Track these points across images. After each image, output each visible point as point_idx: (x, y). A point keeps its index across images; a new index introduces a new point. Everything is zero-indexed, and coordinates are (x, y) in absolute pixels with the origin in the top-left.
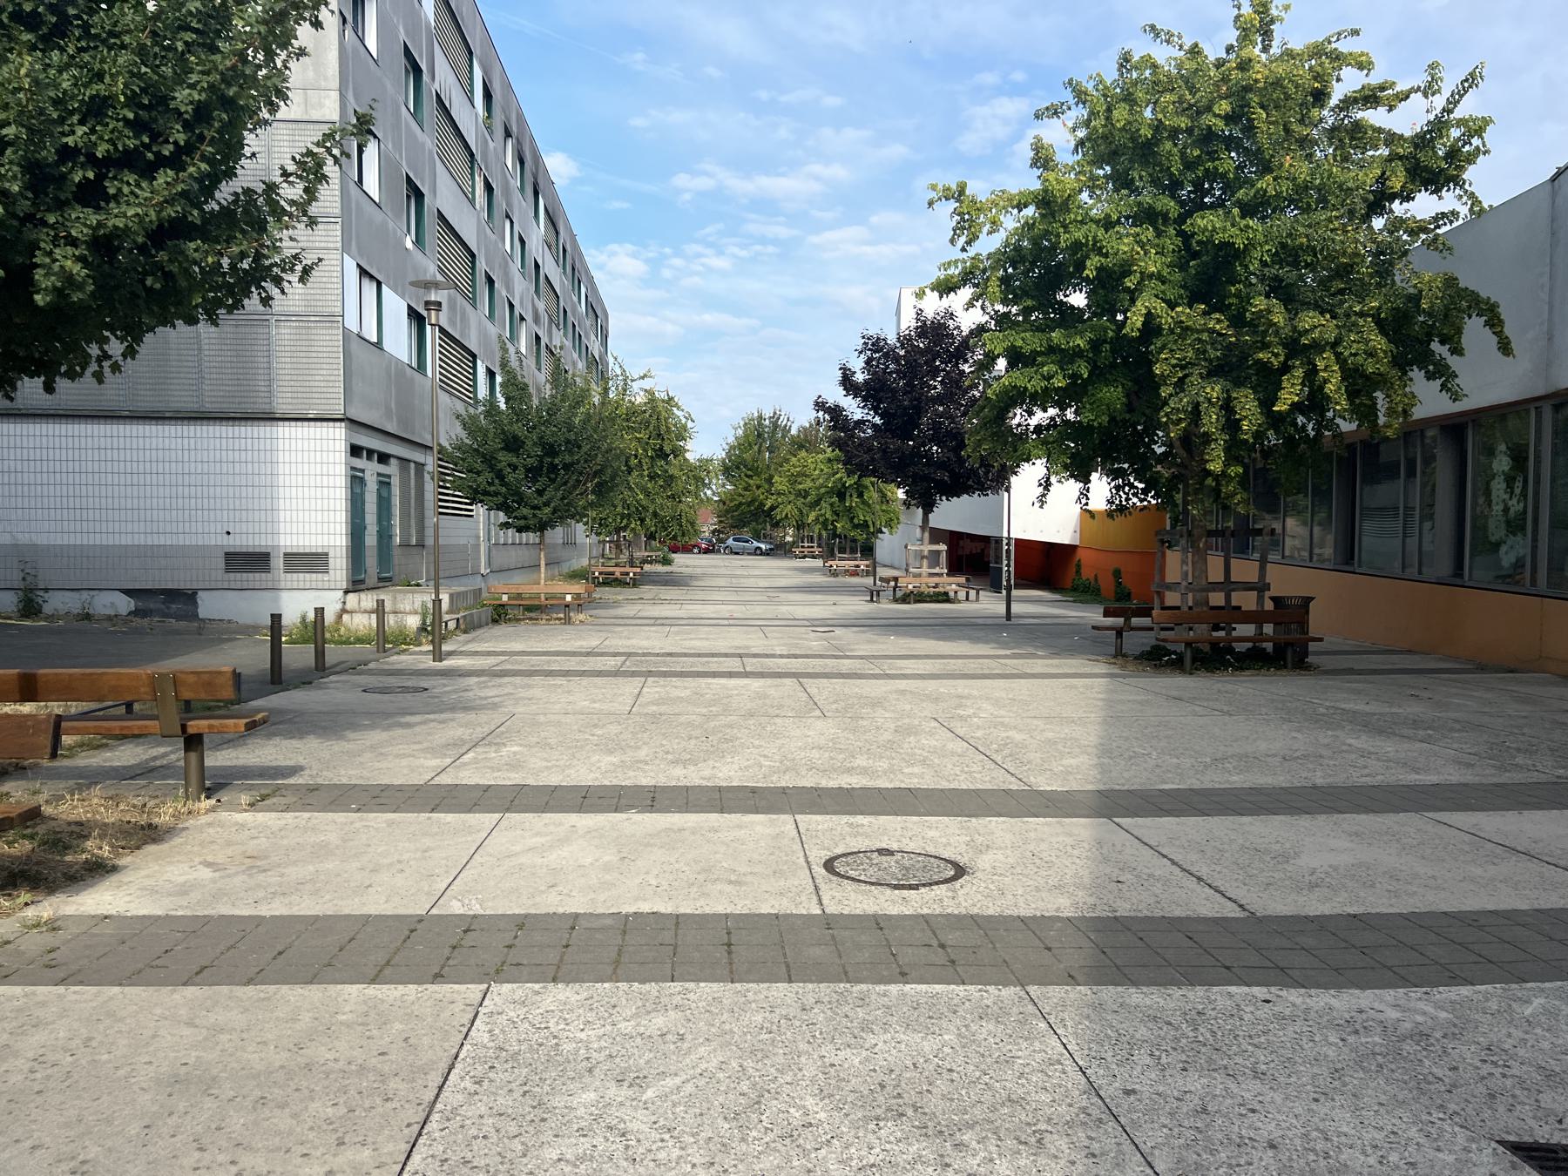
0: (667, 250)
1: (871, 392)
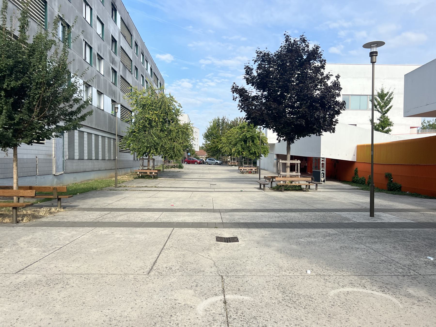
0: (198, 81)
1: (261, 82)
